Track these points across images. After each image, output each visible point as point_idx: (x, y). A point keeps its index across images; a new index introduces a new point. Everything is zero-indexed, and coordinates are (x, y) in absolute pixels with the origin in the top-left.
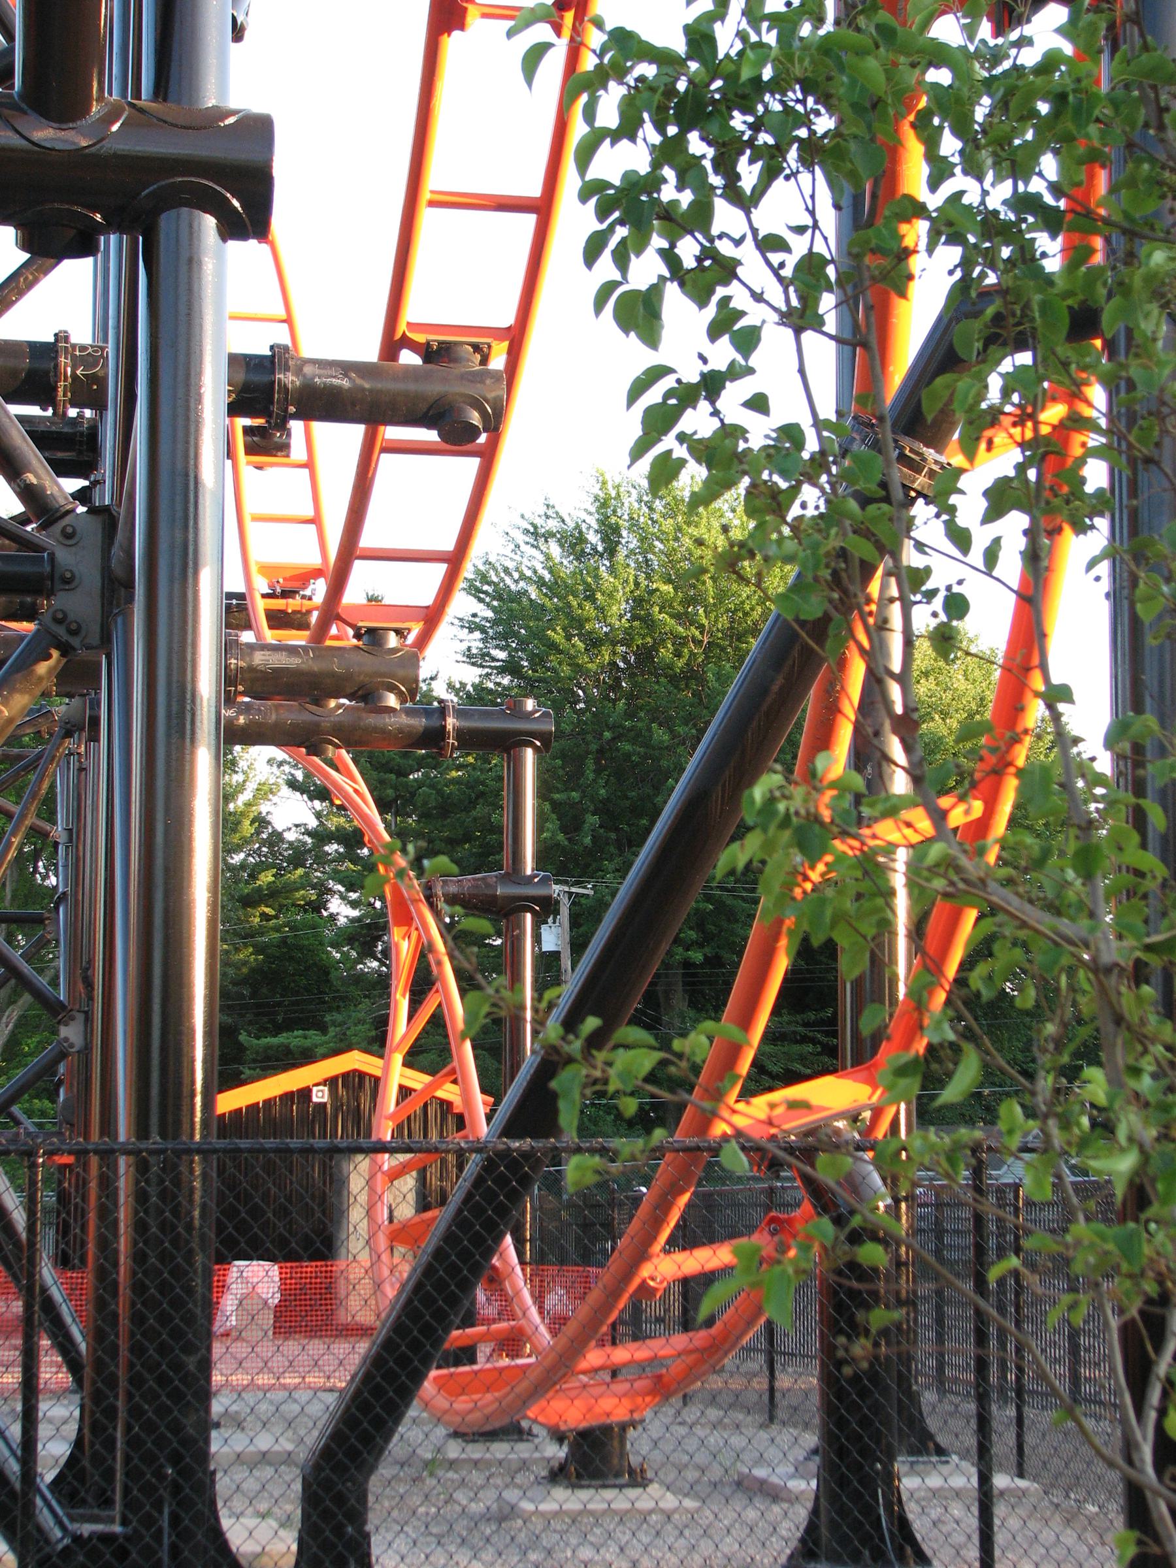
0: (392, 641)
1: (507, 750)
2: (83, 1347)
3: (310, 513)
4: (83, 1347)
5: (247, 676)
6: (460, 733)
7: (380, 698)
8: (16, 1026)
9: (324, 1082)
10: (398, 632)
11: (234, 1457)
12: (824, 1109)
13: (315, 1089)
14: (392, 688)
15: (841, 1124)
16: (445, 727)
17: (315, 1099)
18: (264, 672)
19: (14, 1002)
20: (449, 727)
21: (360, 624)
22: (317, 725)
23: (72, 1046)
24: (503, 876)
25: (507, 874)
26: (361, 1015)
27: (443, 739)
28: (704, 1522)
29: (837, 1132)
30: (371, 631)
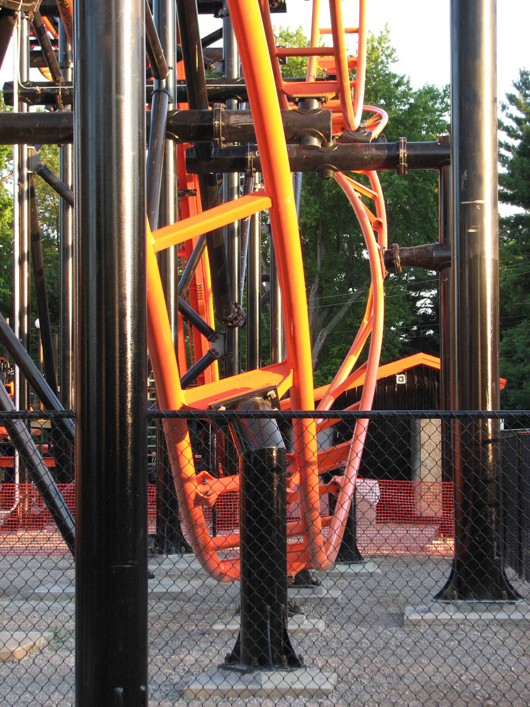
0: (316, 105)
1: (439, 167)
2: (73, 531)
3: (356, 26)
4: (73, 531)
5: (227, 131)
6: (409, 159)
7: (308, 140)
8: (326, 340)
9: (403, 372)
10: (319, 99)
11: (28, 599)
12: (250, 389)
13: (398, 376)
14: (315, 135)
15: (258, 399)
16: (399, 155)
17: (398, 382)
18: (236, 128)
19: (325, 327)
20: (401, 155)
21: (295, 96)
22: (321, 157)
23: (217, 354)
24: (437, 246)
25: (441, 245)
26: (522, 330)
27: (399, 163)
28: (459, 638)
29: (256, 405)
30: (302, 99)
